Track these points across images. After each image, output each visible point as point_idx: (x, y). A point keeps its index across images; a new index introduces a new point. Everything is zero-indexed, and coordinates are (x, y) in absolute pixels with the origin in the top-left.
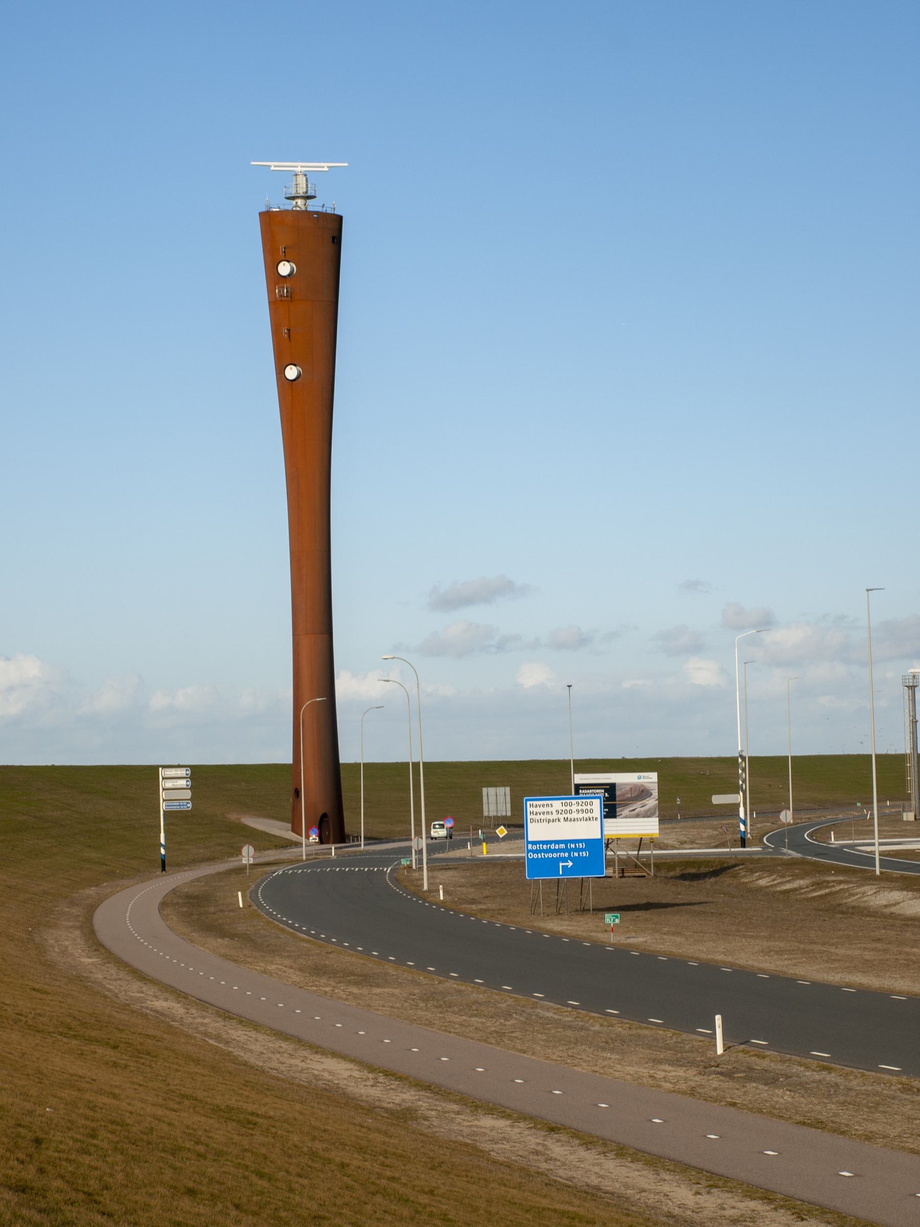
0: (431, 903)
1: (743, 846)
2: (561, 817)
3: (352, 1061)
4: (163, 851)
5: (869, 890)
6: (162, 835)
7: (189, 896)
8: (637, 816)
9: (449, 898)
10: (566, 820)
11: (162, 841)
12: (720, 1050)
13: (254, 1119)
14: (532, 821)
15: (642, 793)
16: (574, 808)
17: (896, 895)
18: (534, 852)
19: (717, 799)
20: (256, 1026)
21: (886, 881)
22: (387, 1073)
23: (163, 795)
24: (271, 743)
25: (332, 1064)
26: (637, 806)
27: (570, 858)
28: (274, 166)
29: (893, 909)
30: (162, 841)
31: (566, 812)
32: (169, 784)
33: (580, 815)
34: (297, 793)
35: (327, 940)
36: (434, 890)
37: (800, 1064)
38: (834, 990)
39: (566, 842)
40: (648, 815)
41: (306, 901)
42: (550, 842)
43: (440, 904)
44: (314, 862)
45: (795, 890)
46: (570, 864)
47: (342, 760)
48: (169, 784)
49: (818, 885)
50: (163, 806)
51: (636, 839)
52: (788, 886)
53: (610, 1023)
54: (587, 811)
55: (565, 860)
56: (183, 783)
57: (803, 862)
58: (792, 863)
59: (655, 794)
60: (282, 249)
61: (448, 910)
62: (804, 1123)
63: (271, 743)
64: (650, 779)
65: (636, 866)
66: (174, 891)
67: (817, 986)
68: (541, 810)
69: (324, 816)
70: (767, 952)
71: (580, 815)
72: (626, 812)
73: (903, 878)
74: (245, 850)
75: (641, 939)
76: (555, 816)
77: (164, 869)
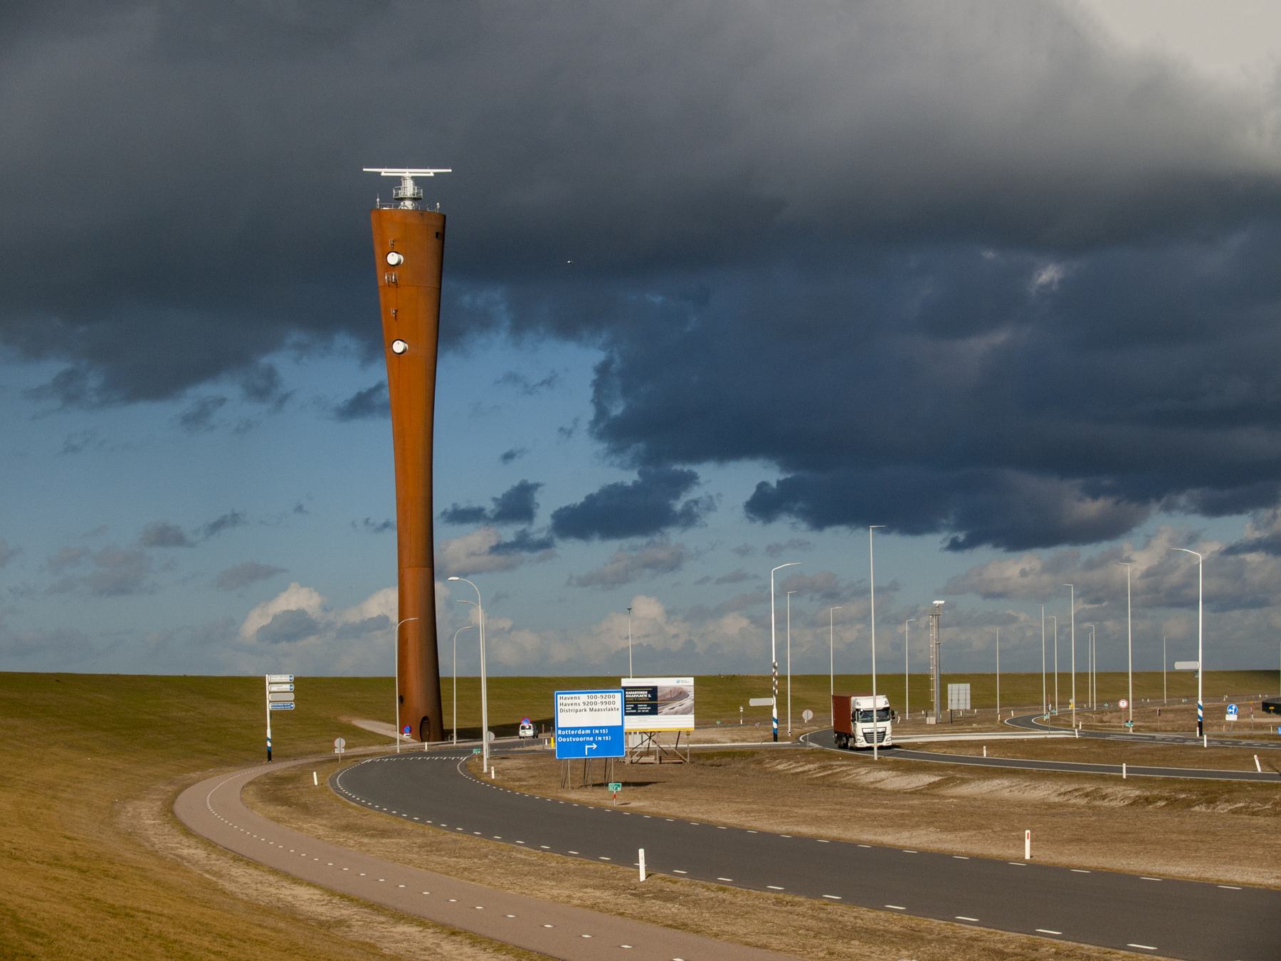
0: (487, 782)
1: (776, 739)
2: (587, 708)
3: (315, 886)
4: (269, 744)
5: (863, 771)
6: (269, 731)
7: (277, 778)
8: (676, 713)
9: (500, 777)
10: (591, 710)
11: (269, 735)
12: (643, 877)
13: (132, 912)
14: (562, 711)
15: (680, 694)
16: (599, 700)
17: (883, 774)
18: (563, 736)
19: (754, 702)
20: (256, 864)
21: (881, 764)
22: (342, 897)
23: (269, 697)
24: (378, 657)
25: (303, 893)
26: (676, 705)
27: (594, 741)
28: (385, 172)
29: (878, 785)
30: (269, 735)
31: (591, 703)
32: (275, 688)
33: (604, 707)
34: (401, 699)
35: (399, 815)
36: (489, 773)
37: (703, 887)
38: (775, 836)
39: (591, 728)
40: (685, 712)
41: (384, 786)
42: (578, 728)
43: (492, 783)
44: (407, 754)
45: (804, 772)
46: (595, 746)
47: (441, 675)
48: (275, 688)
49: (824, 768)
50: (269, 707)
51: (671, 732)
52: (800, 769)
53: (522, 852)
54: (609, 703)
55: (590, 743)
56: (287, 687)
57: (821, 752)
58: (813, 752)
59: (692, 695)
60: (390, 242)
61: (498, 787)
62: (670, 926)
63: (378, 657)
64: (688, 683)
65: (675, 755)
66: (266, 775)
67: (763, 834)
68: (567, 701)
69: (425, 718)
70: (738, 812)
71: (604, 707)
72: (666, 709)
73: (895, 762)
74: (337, 742)
75: (641, 804)
76: (582, 707)
77: (270, 758)
